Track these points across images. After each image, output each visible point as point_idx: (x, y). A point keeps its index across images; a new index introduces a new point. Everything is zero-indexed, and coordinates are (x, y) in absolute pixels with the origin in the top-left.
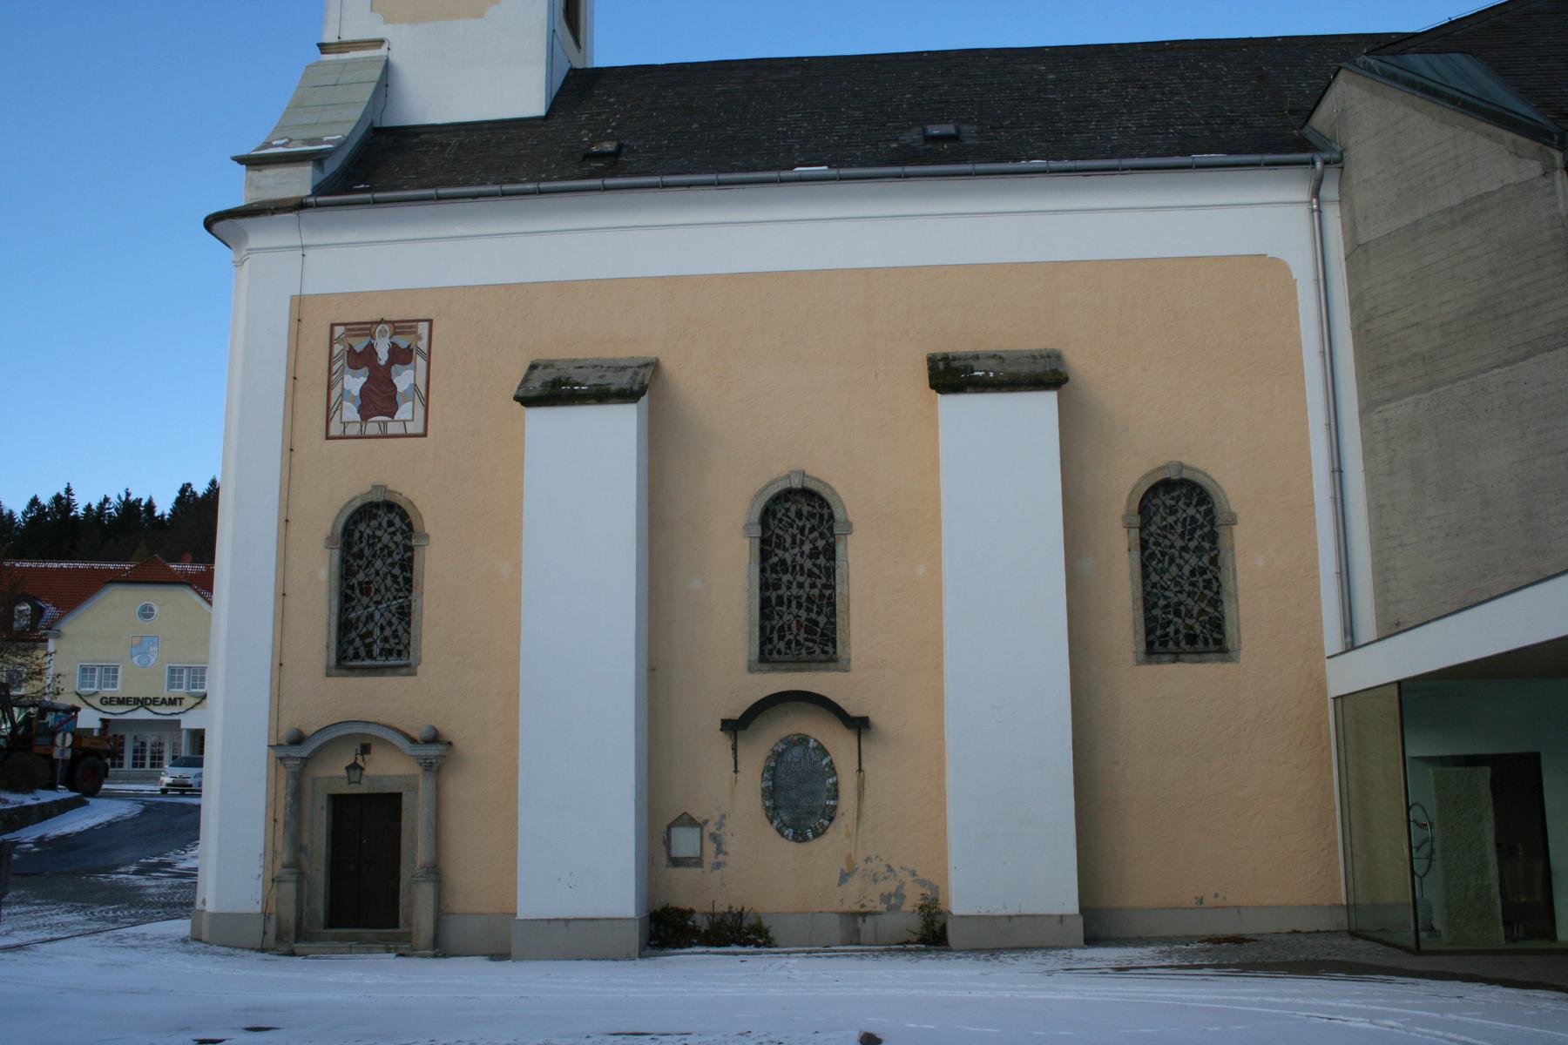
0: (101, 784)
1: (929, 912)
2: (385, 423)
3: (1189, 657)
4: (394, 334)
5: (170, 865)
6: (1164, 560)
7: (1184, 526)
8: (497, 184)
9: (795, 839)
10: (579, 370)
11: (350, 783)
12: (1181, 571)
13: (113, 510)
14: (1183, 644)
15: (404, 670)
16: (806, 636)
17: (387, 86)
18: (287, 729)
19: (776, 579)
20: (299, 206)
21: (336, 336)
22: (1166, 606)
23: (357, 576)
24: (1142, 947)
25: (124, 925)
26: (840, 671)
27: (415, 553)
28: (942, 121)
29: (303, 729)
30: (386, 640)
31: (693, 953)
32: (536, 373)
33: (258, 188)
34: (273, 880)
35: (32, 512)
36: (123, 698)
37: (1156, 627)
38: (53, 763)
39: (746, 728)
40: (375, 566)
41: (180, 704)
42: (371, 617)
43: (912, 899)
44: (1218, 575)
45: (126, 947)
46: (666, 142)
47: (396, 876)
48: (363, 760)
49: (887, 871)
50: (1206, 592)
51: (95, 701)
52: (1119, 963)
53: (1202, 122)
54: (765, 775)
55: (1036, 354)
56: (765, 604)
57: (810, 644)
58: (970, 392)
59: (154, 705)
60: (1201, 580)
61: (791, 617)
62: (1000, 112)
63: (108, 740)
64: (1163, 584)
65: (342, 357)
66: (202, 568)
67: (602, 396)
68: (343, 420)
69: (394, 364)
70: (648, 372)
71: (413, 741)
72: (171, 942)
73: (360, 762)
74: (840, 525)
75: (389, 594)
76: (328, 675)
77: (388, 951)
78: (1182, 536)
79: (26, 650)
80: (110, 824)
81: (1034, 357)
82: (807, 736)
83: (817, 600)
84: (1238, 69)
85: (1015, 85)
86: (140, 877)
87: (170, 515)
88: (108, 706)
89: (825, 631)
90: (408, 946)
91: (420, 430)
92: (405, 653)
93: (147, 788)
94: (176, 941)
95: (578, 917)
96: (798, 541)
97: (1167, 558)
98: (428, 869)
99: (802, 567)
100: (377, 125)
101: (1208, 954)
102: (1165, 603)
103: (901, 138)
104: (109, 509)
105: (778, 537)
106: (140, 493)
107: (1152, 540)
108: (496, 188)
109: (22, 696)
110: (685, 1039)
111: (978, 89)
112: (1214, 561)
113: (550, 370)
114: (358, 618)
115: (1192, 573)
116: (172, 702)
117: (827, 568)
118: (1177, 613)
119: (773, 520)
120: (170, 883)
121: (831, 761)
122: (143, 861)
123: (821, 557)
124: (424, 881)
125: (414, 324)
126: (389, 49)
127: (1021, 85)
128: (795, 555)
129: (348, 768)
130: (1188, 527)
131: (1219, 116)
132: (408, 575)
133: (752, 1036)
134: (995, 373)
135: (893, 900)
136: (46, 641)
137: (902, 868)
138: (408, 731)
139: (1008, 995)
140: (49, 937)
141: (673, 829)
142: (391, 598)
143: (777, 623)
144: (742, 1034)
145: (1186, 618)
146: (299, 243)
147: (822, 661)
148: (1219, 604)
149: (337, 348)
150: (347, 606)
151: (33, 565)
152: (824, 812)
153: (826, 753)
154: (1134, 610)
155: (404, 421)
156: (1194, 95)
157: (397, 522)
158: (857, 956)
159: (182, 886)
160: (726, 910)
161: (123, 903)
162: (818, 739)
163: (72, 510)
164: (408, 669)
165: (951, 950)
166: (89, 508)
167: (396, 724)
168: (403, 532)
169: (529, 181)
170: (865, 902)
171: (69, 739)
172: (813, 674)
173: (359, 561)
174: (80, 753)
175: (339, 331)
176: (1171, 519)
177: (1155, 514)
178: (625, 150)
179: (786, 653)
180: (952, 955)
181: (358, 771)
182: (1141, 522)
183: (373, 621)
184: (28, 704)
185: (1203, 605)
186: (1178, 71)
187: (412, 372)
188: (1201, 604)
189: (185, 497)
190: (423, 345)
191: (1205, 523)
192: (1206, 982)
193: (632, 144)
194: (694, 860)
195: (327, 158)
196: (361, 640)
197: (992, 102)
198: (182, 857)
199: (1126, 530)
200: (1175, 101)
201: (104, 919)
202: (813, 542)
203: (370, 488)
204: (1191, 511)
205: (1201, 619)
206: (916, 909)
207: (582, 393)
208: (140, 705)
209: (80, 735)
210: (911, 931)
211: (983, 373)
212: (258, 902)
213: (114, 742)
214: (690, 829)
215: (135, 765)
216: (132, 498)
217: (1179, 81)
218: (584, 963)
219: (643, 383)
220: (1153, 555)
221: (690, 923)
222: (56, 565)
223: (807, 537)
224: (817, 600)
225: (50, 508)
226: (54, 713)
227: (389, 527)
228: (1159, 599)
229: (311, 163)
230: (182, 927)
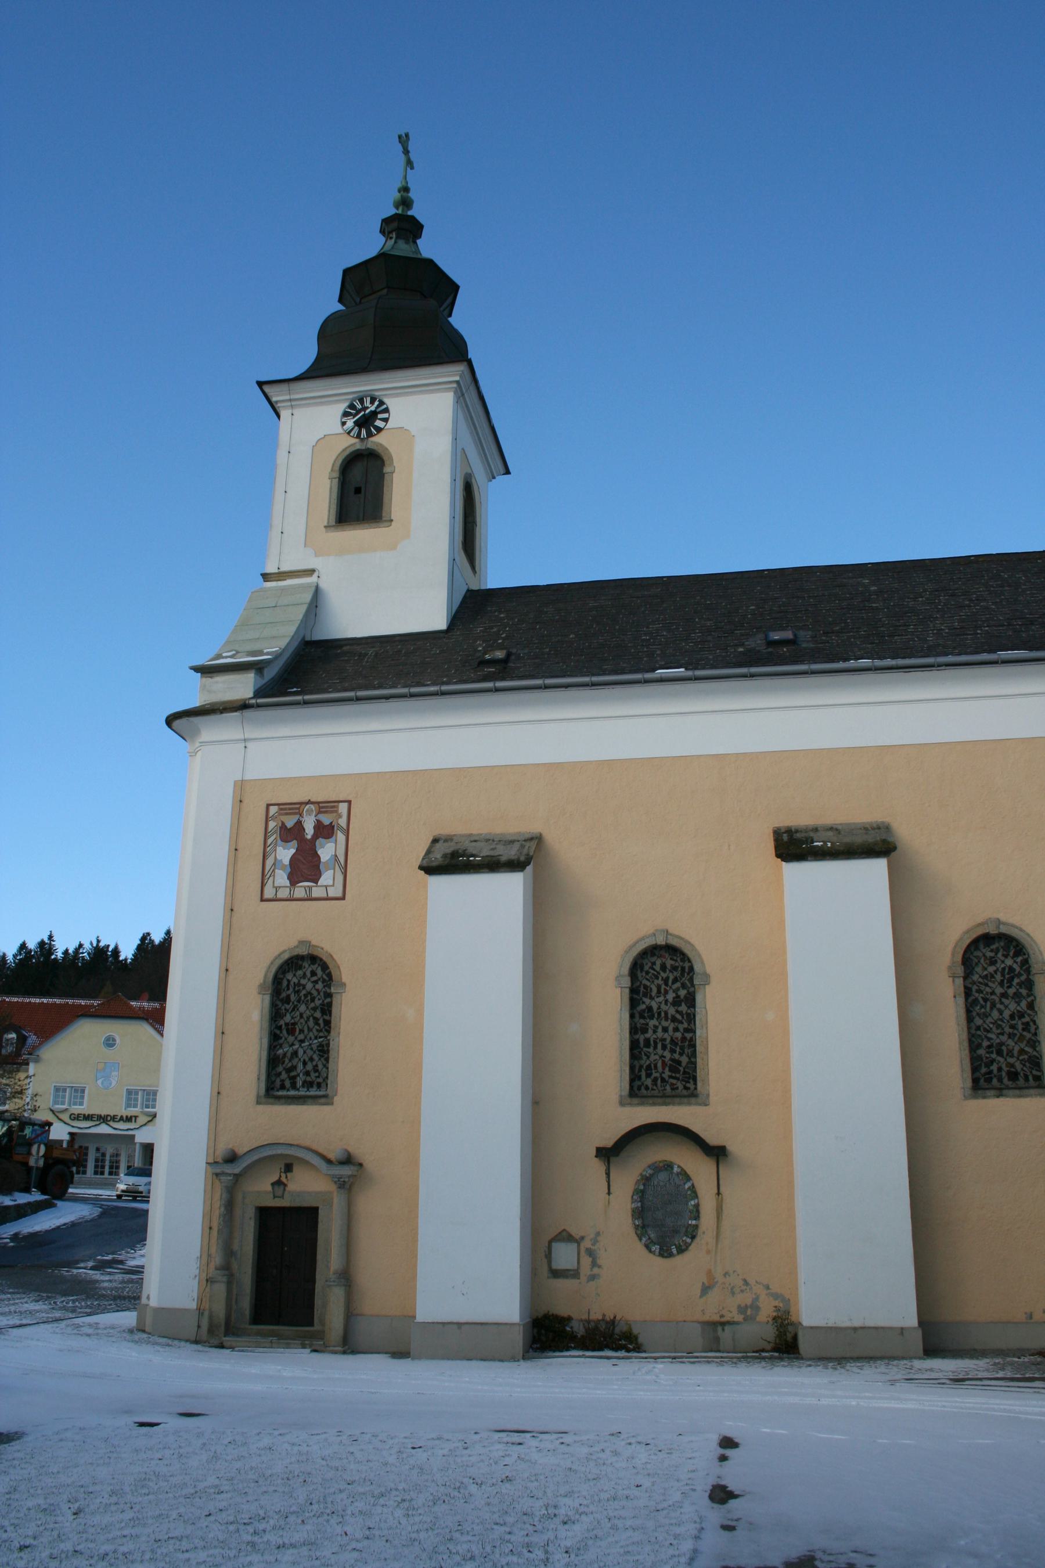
0: (67, 1188)
1: (782, 1323)
2: (310, 888)
3: (1011, 1092)
4: (318, 813)
5: (121, 1262)
6: (986, 1005)
7: (1003, 975)
8: (407, 687)
9: (661, 1255)
10: (474, 844)
11: (275, 1197)
12: (1001, 1014)
13: (85, 954)
14: (1006, 1081)
15: (323, 1100)
16: (670, 1074)
17: (316, 607)
18: (222, 1149)
19: (643, 1024)
20: (243, 706)
21: (271, 814)
22: (989, 1047)
23: (284, 1018)
24: (977, 1359)
25: (81, 1315)
26: (700, 1105)
27: (334, 999)
28: (783, 629)
29: (236, 1150)
30: (307, 1073)
31: (571, 1356)
32: (438, 845)
33: (210, 692)
34: (207, 1280)
35: (21, 954)
36: (89, 1115)
37: (980, 1065)
38: (29, 1169)
39: (617, 1155)
40: (300, 1009)
41: (135, 1121)
42: (295, 1053)
43: (767, 1310)
44: (1035, 1019)
45: (82, 1335)
46: (547, 650)
47: (312, 1280)
48: (286, 1177)
49: (743, 1285)
50: (1025, 1033)
51: (65, 1117)
52: (956, 1374)
53: (1006, 624)
54: (634, 1197)
55: (868, 826)
56: (634, 1045)
57: (674, 1081)
58: (811, 861)
59: (114, 1121)
60: (1020, 1023)
61: (657, 1057)
62: (831, 619)
63: (75, 1152)
64: (986, 1026)
65: (275, 832)
66: (157, 1005)
67: (493, 865)
68: (275, 885)
69: (318, 838)
70: (533, 845)
71: (329, 1161)
72: (120, 1332)
73: (283, 1179)
74: (699, 976)
75: (311, 1034)
76: (258, 1103)
77: (304, 1347)
78: (1001, 984)
79: (11, 1072)
80: (73, 1225)
81: (866, 829)
82: (671, 1162)
83: (679, 1043)
84: (1035, 578)
85: (843, 596)
86: (96, 1272)
87: (131, 959)
88: (76, 1121)
89: (686, 1070)
90: (322, 1343)
91: (340, 894)
92: (324, 1085)
93: (105, 1193)
94: (124, 1331)
95: (470, 1321)
96: (662, 991)
97: (988, 1004)
98: (340, 1275)
99: (666, 1013)
100: (308, 639)
101: (1038, 1366)
102: (988, 1043)
103: (747, 643)
104: (83, 953)
105: (646, 987)
106: (108, 941)
107: (975, 988)
108: (405, 690)
109: (7, 1111)
110: (562, 1438)
111: (811, 600)
112: (1031, 1006)
113: (449, 844)
114: (285, 1055)
115: (1012, 1017)
116: (128, 1119)
117: (688, 1015)
118: (999, 1053)
119: (641, 972)
120: (121, 1278)
121: (693, 1185)
122: (99, 1257)
123: (683, 1004)
124: (336, 1285)
125: (336, 804)
126: (319, 577)
127: (848, 596)
128: (661, 1003)
129: (273, 1184)
130: (1007, 976)
131: (1019, 618)
132: (327, 1018)
133: (622, 1436)
134: (832, 843)
135: (748, 1312)
136: (28, 1064)
137: (757, 1282)
138: (325, 1153)
139: (854, 1403)
140: (18, 1322)
141: (555, 1246)
142: (313, 1037)
143: (645, 1062)
144: (613, 1435)
145: (1008, 1057)
146: (242, 737)
147: (685, 1096)
148: (1037, 1044)
149: (272, 824)
150: (276, 1043)
151: (20, 1000)
152: (686, 1231)
153: (688, 1178)
154: (960, 1050)
155: (326, 887)
156: (998, 600)
157: (319, 972)
158: (717, 1362)
159: (131, 1281)
160: (600, 1318)
161: (81, 1295)
162: (682, 1165)
163: (53, 954)
164: (326, 1099)
165: (802, 1359)
166: (66, 952)
167: (315, 1147)
168: (324, 981)
169: (434, 684)
170: (724, 1312)
171: (43, 1148)
172: (676, 1108)
173: (286, 1006)
174: (51, 1161)
175: (273, 810)
176: (991, 969)
177: (977, 964)
178: (513, 657)
179: (652, 1089)
180: (803, 1363)
181: (282, 1187)
182: (965, 972)
183: (297, 1057)
184: (10, 1118)
185: (1022, 1045)
186: (983, 581)
187: (334, 845)
188: (1021, 1045)
189: (145, 945)
190: (343, 822)
191: (1022, 972)
192: (1038, 1395)
193: (519, 652)
194: (572, 1273)
195: (266, 667)
196: (286, 1072)
197: (824, 611)
198: (132, 1256)
199: (951, 979)
200: (981, 606)
201: (64, 1308)
202: (676, 991)
203: (296, 943)
204: (1009, 962)
205: (1021, 1058)
206: (770, 1320)
207: (476, 862)
208: (102, 1121)
209: (52, 1146)
210: (766, 1340)
211: (822, 843)
212: (194, 1300)
213: (80, 1154)
214: (569, 1244)
215: (96, 1173)
216: (102, 944)
217: (984, 589)
218: (474, 1363)
219: (528, 855)
220: (976, 1001)
221: (568, 1329)
222: (38, 1001)
223: (671, 987)
224: (679, 1043)
225: (35, 952)
226: (31, 1127)
227: (312, 976)
228: (982, 1040)
229: (254, 671)
230: (128, 1318)
